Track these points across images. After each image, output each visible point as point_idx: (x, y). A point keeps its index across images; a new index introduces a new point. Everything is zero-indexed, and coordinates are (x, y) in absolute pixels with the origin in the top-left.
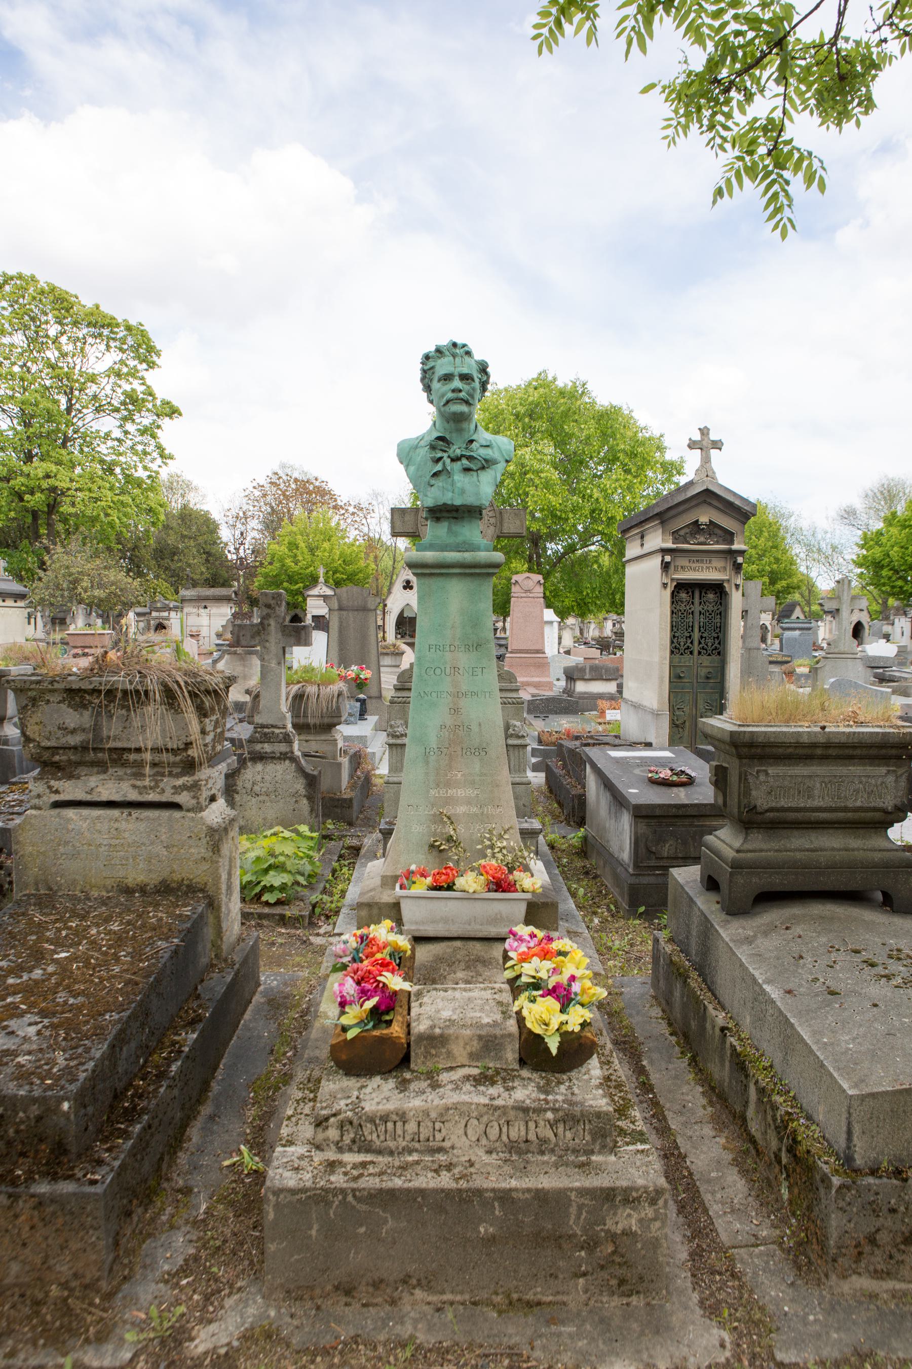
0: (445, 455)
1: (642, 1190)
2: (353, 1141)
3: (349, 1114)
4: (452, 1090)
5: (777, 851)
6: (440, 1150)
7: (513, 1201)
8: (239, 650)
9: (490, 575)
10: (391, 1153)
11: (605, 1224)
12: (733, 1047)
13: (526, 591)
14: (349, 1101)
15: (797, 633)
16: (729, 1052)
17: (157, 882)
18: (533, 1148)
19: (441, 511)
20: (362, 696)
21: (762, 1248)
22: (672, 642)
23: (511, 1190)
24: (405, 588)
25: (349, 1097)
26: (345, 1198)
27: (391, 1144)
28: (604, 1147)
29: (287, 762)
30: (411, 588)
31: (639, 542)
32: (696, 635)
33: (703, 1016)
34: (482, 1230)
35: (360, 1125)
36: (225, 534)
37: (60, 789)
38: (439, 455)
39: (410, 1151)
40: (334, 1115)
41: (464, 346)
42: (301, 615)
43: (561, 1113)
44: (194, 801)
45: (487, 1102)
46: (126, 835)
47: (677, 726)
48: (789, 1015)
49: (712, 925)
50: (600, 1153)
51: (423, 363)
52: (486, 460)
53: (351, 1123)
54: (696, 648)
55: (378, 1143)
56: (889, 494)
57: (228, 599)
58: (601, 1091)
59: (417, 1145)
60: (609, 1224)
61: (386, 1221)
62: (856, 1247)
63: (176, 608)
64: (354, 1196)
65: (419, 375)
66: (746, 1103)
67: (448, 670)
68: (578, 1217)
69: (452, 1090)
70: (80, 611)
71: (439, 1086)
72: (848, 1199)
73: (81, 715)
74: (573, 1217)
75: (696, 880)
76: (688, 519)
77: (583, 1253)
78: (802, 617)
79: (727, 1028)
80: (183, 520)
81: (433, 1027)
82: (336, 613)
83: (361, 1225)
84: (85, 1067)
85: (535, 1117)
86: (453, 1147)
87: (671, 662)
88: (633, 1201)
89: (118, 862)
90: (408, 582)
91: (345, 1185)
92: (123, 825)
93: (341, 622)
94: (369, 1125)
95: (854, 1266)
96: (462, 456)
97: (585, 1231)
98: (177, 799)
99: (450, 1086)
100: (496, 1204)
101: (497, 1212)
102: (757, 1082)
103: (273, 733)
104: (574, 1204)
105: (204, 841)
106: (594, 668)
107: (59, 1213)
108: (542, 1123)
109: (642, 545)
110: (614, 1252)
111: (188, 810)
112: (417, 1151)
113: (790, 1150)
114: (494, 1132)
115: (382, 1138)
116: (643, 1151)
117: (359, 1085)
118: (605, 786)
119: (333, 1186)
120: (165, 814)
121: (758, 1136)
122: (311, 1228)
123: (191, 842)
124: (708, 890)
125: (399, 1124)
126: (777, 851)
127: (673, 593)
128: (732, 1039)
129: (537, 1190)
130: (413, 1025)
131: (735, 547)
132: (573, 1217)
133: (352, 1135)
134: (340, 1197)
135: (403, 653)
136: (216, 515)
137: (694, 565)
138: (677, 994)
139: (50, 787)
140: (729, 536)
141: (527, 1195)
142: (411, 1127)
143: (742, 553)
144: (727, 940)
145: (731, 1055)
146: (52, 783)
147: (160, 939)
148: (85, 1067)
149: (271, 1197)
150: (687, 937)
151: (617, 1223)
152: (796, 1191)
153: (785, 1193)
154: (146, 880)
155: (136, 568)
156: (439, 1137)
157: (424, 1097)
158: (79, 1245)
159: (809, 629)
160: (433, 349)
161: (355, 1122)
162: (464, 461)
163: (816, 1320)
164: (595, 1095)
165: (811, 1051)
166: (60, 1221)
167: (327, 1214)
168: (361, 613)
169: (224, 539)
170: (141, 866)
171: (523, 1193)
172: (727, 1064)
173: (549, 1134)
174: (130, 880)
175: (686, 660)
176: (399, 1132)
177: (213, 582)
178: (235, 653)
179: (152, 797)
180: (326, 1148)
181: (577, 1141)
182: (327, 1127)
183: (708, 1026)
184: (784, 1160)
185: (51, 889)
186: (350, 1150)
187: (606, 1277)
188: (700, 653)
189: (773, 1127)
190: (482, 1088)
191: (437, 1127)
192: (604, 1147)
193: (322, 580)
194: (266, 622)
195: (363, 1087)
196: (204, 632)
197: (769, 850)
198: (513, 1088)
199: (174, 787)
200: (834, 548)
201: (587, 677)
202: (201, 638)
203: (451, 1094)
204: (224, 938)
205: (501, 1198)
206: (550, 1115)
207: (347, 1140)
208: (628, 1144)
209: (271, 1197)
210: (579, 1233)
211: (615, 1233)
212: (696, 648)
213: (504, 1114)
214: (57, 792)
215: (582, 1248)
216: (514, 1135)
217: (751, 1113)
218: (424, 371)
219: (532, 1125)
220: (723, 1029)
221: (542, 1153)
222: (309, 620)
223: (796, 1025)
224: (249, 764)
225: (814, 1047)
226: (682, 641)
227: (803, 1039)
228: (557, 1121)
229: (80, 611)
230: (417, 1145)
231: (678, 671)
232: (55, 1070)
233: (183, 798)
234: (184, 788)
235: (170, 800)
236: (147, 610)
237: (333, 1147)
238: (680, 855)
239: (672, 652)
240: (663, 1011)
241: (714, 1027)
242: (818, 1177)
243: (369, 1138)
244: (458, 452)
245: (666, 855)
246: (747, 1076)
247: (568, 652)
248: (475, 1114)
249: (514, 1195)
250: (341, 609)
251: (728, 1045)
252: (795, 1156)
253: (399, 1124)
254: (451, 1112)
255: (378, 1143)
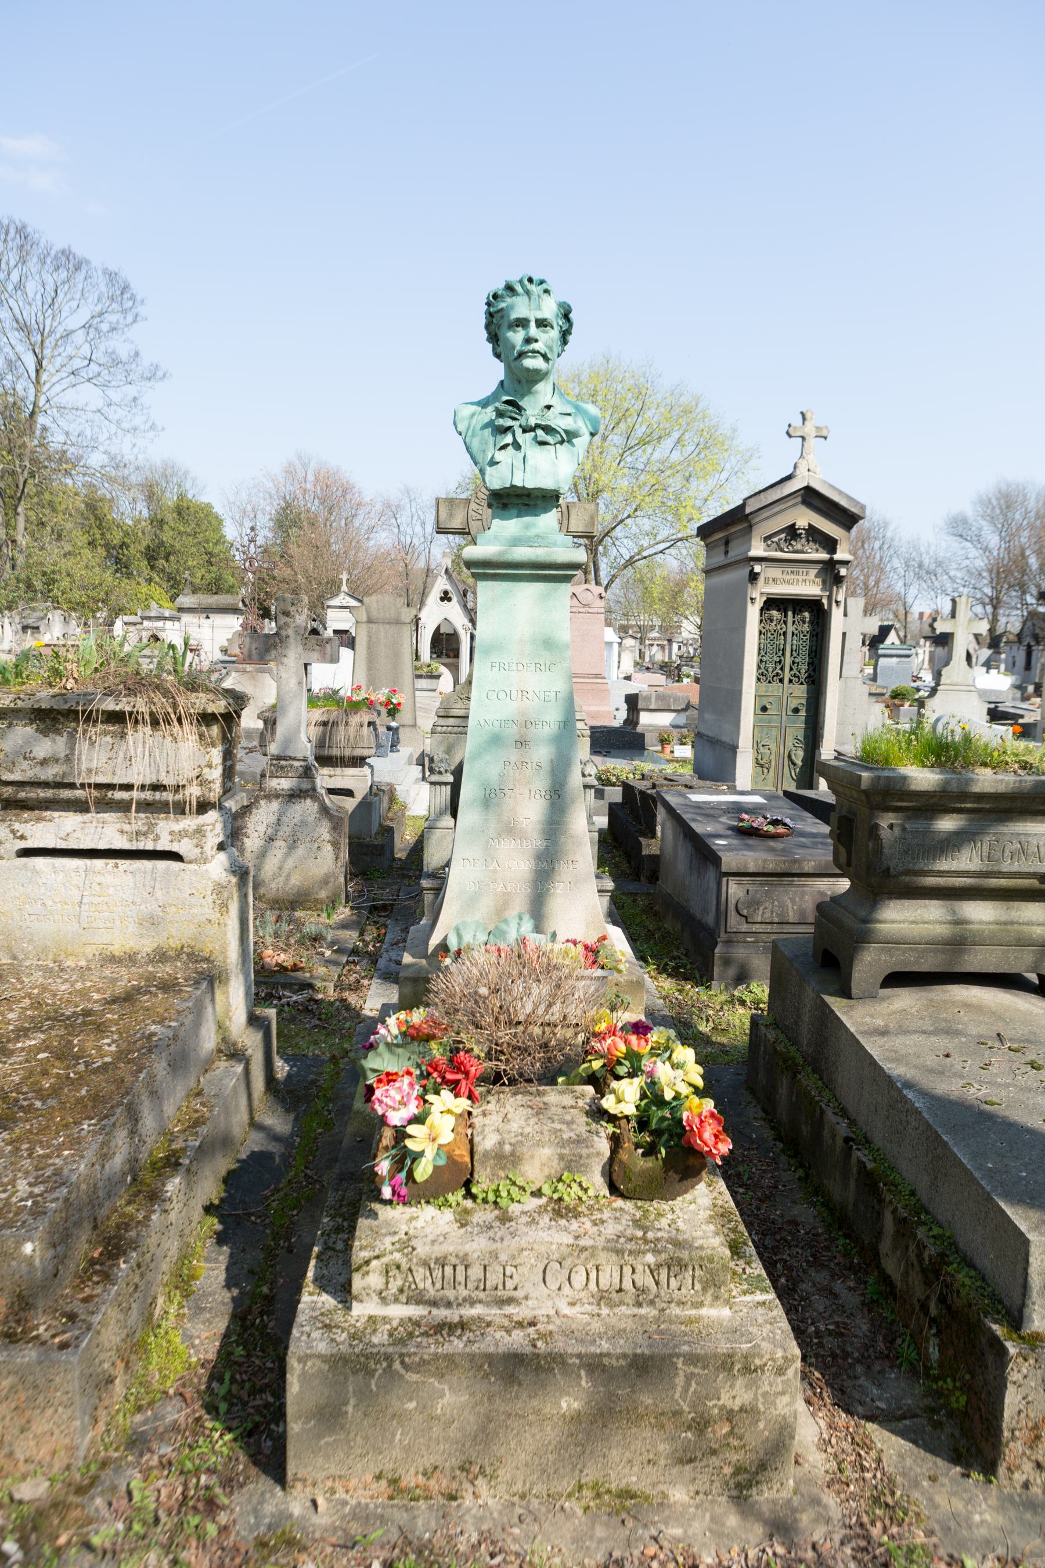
0: (515, 424)
1: (768, 1356)
2: (401, 1291)
3: (397, 1256)
4: (527, 1224)
5: (913, 922)
6: (510, 1301)
7: (604, 1368)
8: (249, 668)
9: (567, 579)
10: (449, 1305)
11: (719, 1399)
12: (861, 1164)
13: (585, 606)
14: (396, 1238)
15: (895, 660)
16: (855, 1170)
17: (149, 950)
18: (629, 1298)
19: (508, 495)
20: (394, 724)
21: (907, 1422)
22: (759, 667)
23: (601, 1355)
24: (442, 599)
25: (395, 1233)
26: (390, 1366)
27: (450, 1294)
28: (717, 1298)
29: (308, 801)
30: (449, 600)
31: (722, 548)
32: (788, 660)
33: (819, 1122)
34: (564, 1405)
35: (410, 1270)
36: (231, 532)
37: (27, 834)
38: (509, 423)
39: (473, 1302)
40: (377, 1257)
41: (542, 282)
42: (320, 628)
43: (664, 1256)
44: (198, 850)
45: (571, 1241)
46: (111, 891)
47: (762, 766)
48: (940, 1131)
49: (832, 1012)
50: (711, 1306)
51: (489, 304)
52: (566, 431)
53: (398, 1267)
54: (787, 675)
55: (432, 1292)
56: (1004, 505)
57: (234, 610)
58: (712, 1227)
59: (482, 1295)
60: (725, 1400)
61: (442, 1395)
62: (1032, 1429)
63: (171, 619)
64: (402, 1362)
65: (482, 320)
66: (879, 1235)
67: (514, 696)
68: (686, 1390)
69: (527, 1224)
70: (57, 618)
71: (510, 1220)
72: (1025, 1371)
73: (54, 741)
74: (679, 1389)
75: (806, 954)
76: (782, 521)
77: (689, 1434)
78: (897, 642)
79: (852, 1140)
80: (179, 514)
81: (501, 1143)
82: (364, 626)
83: (411, 1400)
84: (56, 1195)
85: (631, 1259)
86: (526, 1298)
87: (757, 691)
88: (755, 1370)
89: (102, 925)
90: (446, 593)
91: (390, 1350)
92: (108, 879)
93: (370, 637)
94: (421, 1270)
95: (1028, 1452)
96: (538, 426)
97: (693, 1406)
98: (175, 847)
99: (524, 1219)
100: (583, 1373)
101: (583, 1383)
102: (894, 1211)
103: (291, 766)
104: (681, 1373)
105: (210, 899)
106: (660, 697)
107: (20, 1387)
108: (639, 1268)
109: (726, 553)
110: (731, 1433)
111: (190, 862)
112: (480, 1302)
113: (942, 1300)
114: (579, 1279)
115: (438, 1285)
116: (764, 1303)
117: (407, 1216)
118: (685, 836)
119: (375, 1350)
120: (162, 864)
121: (896, 1277)
122: (346, 1404)
123: (193, 900)
124: (822, 966)
125: (460, 1269)
126: (913, 922)
127: (762, 610)
128: (859, 1153)
129: (635, 1355)
130: (476, 1139)
131: (837, 556)
132: (679, 1389)
133: (399, 1283)
134: (385, 1364)
135: (438, 677)
136: (218, 509)
137: (787, 577)
138: (783, 1091)
139: (13, 832)
140: (830, 544)
141: (622, 1362)
142: (476, 1272)
143: (846, 563)
144: (852, 1030)
145: (859, 1172)
146: (17, 826)
147: (154, 1022)
148: (56, 1195)
149: (296, 1364)
150: (796, 1023)
151: (734, 1397)
152: (950, 1352)
153: (934, 1353)
154: (136, 948)
155: (122, 566)
156: (510, 1284)
157: (491, 1233)
158: (46, 1427)
159: (909, 656)
160: (502, 285)
161: (405, 1266)
162: (540, 432)
163: (982, 1521)
164: (705, 1232)
165: (973, 1180)
166: (23, 1396)
167: (369, 1386)
168: (393, 627)
169: (229, 538)
170: (130, 929)
171: (617, 1359)
172: (852, 1184)
173: (650, 1282)
174: (117, 946)
175: (775, 688)
176: (461, 1278)
177: (216, 587)
178: (245, 671)
179: (149, 846)
180: (365, 1298)
181: (683, 1290)
182: (368, 1273)
183: (826, 1133)
184: (933, 1311)
185: (15, 958)
186: (396, 1300)
187: (718, 1464)
188: (791, 681)
189: (917, 1268)
190: (563, 1222)
191: (508, 1273)
192: (717, 1298)
193: (344, 588)
194: (284, 633)
195: (412, 1219)
196: (207, 646)
197: (904, 922)
198: (602, 1222)
199: (171, 833)
200: (939, 564)
201: (652, 707)
202: (202, 652)
203: (525, 1229)
204: (234, 1019)
205: (589, 1365)
206: (650, 1258)
207: (394, 1286)
208: (745, 1293)
209: (296, 1364)
210: (686, 1409)
211: (732, 1410)
212: (787, 675)
213: (593, 1256)
214: (22, 837)
215: (689, 1428)
216: (604, 1283)
217: (885, 1246)
218: (490, 315)
219: (627, 1270)
220: (847, 1140)
221: (639, 1305)
222: (329, 633)
223: (951, 1143)
224: (262, 802)
225: (977, 1174)
226: (770, 666)
227: (961, 1163)
228: (659, 1266)
229: (57, 618)
230: (482, 1295)
231: (765, 702)
232: (14, 1200)
233: (182, 847)
234: (182, 834)
235: (167, 849)
236: (137, 619)
237: (376, 1298)
238: (776, 920)
239: (759, 679)
240: (764, 1110)
241: (834, 1137)
242: (984, 1340)
243: (421, 1286)
244: (532, 422)
245: (759, 919)
246: (881, 1201)
247: (628, 678)
248: (556, 1256)
249: (606, 1361)
250: (370, 621)
251: (854, 1160)
252: (949, 1308)
253: (460, 1269)
254: (525, 1253)
255: (432, 1292)
